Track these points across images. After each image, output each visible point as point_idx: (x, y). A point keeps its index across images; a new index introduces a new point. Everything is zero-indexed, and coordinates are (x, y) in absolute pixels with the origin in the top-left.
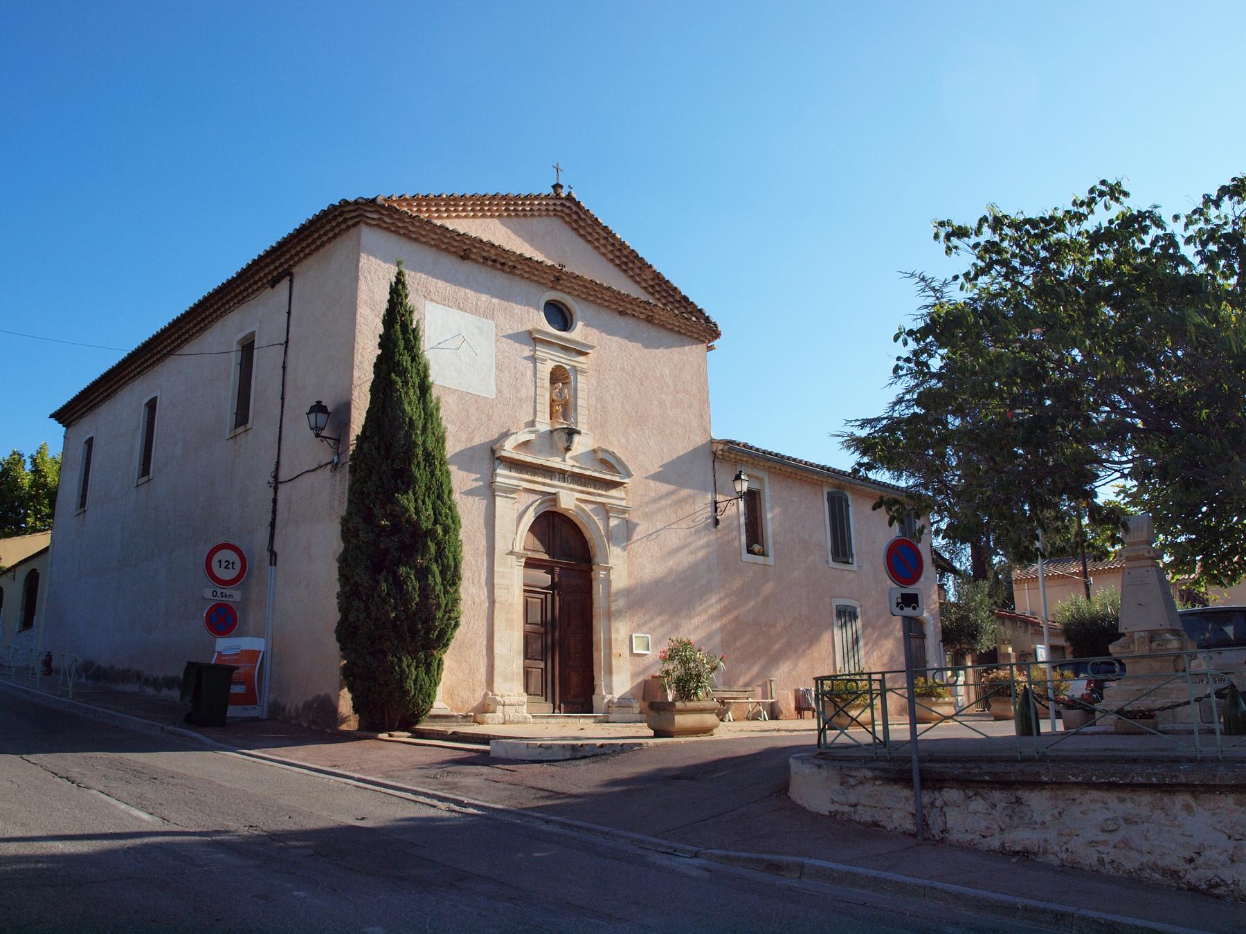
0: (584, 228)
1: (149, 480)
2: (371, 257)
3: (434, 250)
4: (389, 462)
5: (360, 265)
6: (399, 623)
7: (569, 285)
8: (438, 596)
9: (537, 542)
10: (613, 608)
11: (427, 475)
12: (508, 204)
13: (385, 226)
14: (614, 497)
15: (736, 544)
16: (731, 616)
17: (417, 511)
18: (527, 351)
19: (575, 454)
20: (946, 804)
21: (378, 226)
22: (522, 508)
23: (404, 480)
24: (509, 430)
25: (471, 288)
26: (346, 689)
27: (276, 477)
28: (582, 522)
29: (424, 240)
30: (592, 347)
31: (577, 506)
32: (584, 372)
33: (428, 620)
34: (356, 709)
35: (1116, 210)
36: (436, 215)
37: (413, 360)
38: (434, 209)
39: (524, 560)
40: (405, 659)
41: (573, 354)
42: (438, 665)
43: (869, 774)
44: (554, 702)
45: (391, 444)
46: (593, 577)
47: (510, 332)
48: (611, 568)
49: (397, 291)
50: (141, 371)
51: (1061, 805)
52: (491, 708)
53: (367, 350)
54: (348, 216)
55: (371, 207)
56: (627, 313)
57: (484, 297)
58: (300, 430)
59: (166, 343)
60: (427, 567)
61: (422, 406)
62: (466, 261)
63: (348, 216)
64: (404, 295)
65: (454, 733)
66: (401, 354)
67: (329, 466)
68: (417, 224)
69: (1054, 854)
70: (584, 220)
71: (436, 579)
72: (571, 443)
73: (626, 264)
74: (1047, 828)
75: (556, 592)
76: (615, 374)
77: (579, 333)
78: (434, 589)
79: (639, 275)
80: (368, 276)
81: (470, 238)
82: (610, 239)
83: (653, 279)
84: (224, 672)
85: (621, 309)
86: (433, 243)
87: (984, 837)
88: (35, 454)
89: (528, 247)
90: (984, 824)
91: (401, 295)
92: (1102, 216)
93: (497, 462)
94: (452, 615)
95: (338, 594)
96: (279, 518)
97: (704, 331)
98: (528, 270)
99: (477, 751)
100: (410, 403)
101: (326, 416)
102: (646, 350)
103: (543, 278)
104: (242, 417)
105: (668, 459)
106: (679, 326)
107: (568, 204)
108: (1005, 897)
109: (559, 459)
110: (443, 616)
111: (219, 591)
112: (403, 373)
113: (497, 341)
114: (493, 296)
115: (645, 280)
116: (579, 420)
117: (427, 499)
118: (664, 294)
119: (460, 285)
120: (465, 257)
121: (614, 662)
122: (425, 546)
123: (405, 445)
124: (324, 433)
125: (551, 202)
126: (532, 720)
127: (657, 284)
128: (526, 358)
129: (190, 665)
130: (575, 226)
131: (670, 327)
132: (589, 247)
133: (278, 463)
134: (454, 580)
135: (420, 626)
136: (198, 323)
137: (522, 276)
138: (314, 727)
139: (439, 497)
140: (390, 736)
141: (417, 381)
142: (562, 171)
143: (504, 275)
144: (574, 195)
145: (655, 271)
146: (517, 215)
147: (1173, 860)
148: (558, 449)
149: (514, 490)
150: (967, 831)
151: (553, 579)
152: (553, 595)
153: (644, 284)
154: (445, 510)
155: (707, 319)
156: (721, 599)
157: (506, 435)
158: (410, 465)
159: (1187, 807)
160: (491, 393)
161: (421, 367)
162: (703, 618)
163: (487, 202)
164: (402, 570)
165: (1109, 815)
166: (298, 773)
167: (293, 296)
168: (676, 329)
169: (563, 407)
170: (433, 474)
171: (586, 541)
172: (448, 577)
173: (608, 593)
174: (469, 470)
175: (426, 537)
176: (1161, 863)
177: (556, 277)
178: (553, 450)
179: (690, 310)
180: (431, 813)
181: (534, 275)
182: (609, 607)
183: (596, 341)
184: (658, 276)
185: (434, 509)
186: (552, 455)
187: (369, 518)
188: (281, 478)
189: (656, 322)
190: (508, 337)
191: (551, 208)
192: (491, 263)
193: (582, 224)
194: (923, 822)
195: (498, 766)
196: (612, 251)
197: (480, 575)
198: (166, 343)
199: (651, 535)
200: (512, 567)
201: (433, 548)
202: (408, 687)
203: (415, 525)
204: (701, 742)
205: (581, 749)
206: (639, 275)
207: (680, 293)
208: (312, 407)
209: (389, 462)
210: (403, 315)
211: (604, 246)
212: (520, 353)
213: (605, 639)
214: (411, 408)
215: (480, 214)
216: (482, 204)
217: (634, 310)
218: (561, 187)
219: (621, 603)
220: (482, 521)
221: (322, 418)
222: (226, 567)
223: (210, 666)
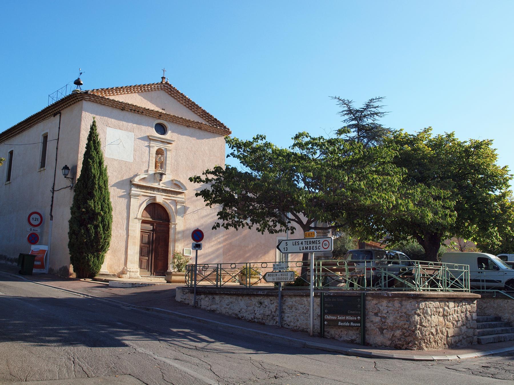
0: (173, 94)
1: (10, 183)
3: (111, 108)
4: (86, 189)
5: (82, 116)
7: (165, 117)
8: (101, 235)
9: (148, 214)
11: (99, 194)
12: (141, 88)
14: (179, 198)
16: (227, 242)
17: (95, 207)
18: (147, 143)
21: (89, 101)
23: (91, 196)
24: (138, 174)
25: (125, 121)
27: (53, 189)
29: (107, 104)
30: (174, 141)
31: (163, 201)
32: (170, 150)
33: (98, 242)
34: (74, 271)
37: (97, 153)
38: (111, 93)
39: (141, 221)
40: (89, 255)
41: (166, 143)
42: (102, 257)
43: (188, 291)
44: (151, 272)
47: (140, 137)
48: (177, 224)
49: (93, 128)
50: (7, 139)
51: (221, 299)
52: (125, 273)
53: (82, 149)
54: (78, 97)
57: (130, 124)
58: (60, 173)
59: (16, 130)
60: (98, 225)
63: (78, 97)
65: (105, 280)
66: (92, 152)
67: (70, 187)
68: (104, 99)
70: (173, 91)
71: (101, 229)
75: (154, 232)
76: (183, 150)
77: (169, 136)
78: (100, 232)
79: (197, 111)
81: (124, 103)
84: (32, 257)
85: (187, 125)
86: (110, 105)
89: (150, 103)
90: (208, 304)
91: (94, 130)
94: (107, 241)
96: (54, 203)
97: (224, 132)
99: (106, 284)
102: (198, 140)
103: (154, 115)
104: (43, 165)
106: (213, 130)
107: (166, 85)
111: (33, 229)
112: (92, 158)
113: (135, 140)
118: (207, 118)
119: (121, 120)
120: (123, 109)
122: (97, 218)
124: (67, 176)
125: (159, 86)
129: (21, 254)
130: (170, 93)
131: (209, 131)
132: (176, 101)
133: (54, 183)
136: (28, 125)
138: (62, 277)
139: (104, 201)
140: (85, 280)
141: (98, 161)
142: (166, 71)
143: (139, 115)
144: (169, 82)
148: (157, 180)
153: (199, 114)
154: (106, 205)
155: (225, 127)
156: (224, 236)
157: (136, 175)
159: (241, 300)
160: (131, 160)
161: (100, 156)
162: (216, 242)
163: (132, 88)
164: (89, 226)
165: (229, 301)
167: (61, 122)
168: (212, 131)
169: (160, 164)
172: (105, 228)
173: (175, 233)
175: (98, 215)
177: (160, 115)
178: (155, 181)
179: (218, 123)
180: (78, 297)
183: (176, 138)
185: (101, 206)
186: (154, 182)
187: (79, 208)
189: (203, 129)
190: (139, 139)
191: (160, 87)
192: (133, 111)
194: (196, 302)
196: (185, 102)
197: (123, 226)
198: (16, 130)
200: (136, 223)
203: (94, 211)
209: (86, 189)
210: (94, 137)
214: (95, 171)
215: (130, 92)
217: (193, 125)
218: (165, 78)
220: (125, 207)
221: (67, 171)
222: (35, 220)
223: (28, 255)
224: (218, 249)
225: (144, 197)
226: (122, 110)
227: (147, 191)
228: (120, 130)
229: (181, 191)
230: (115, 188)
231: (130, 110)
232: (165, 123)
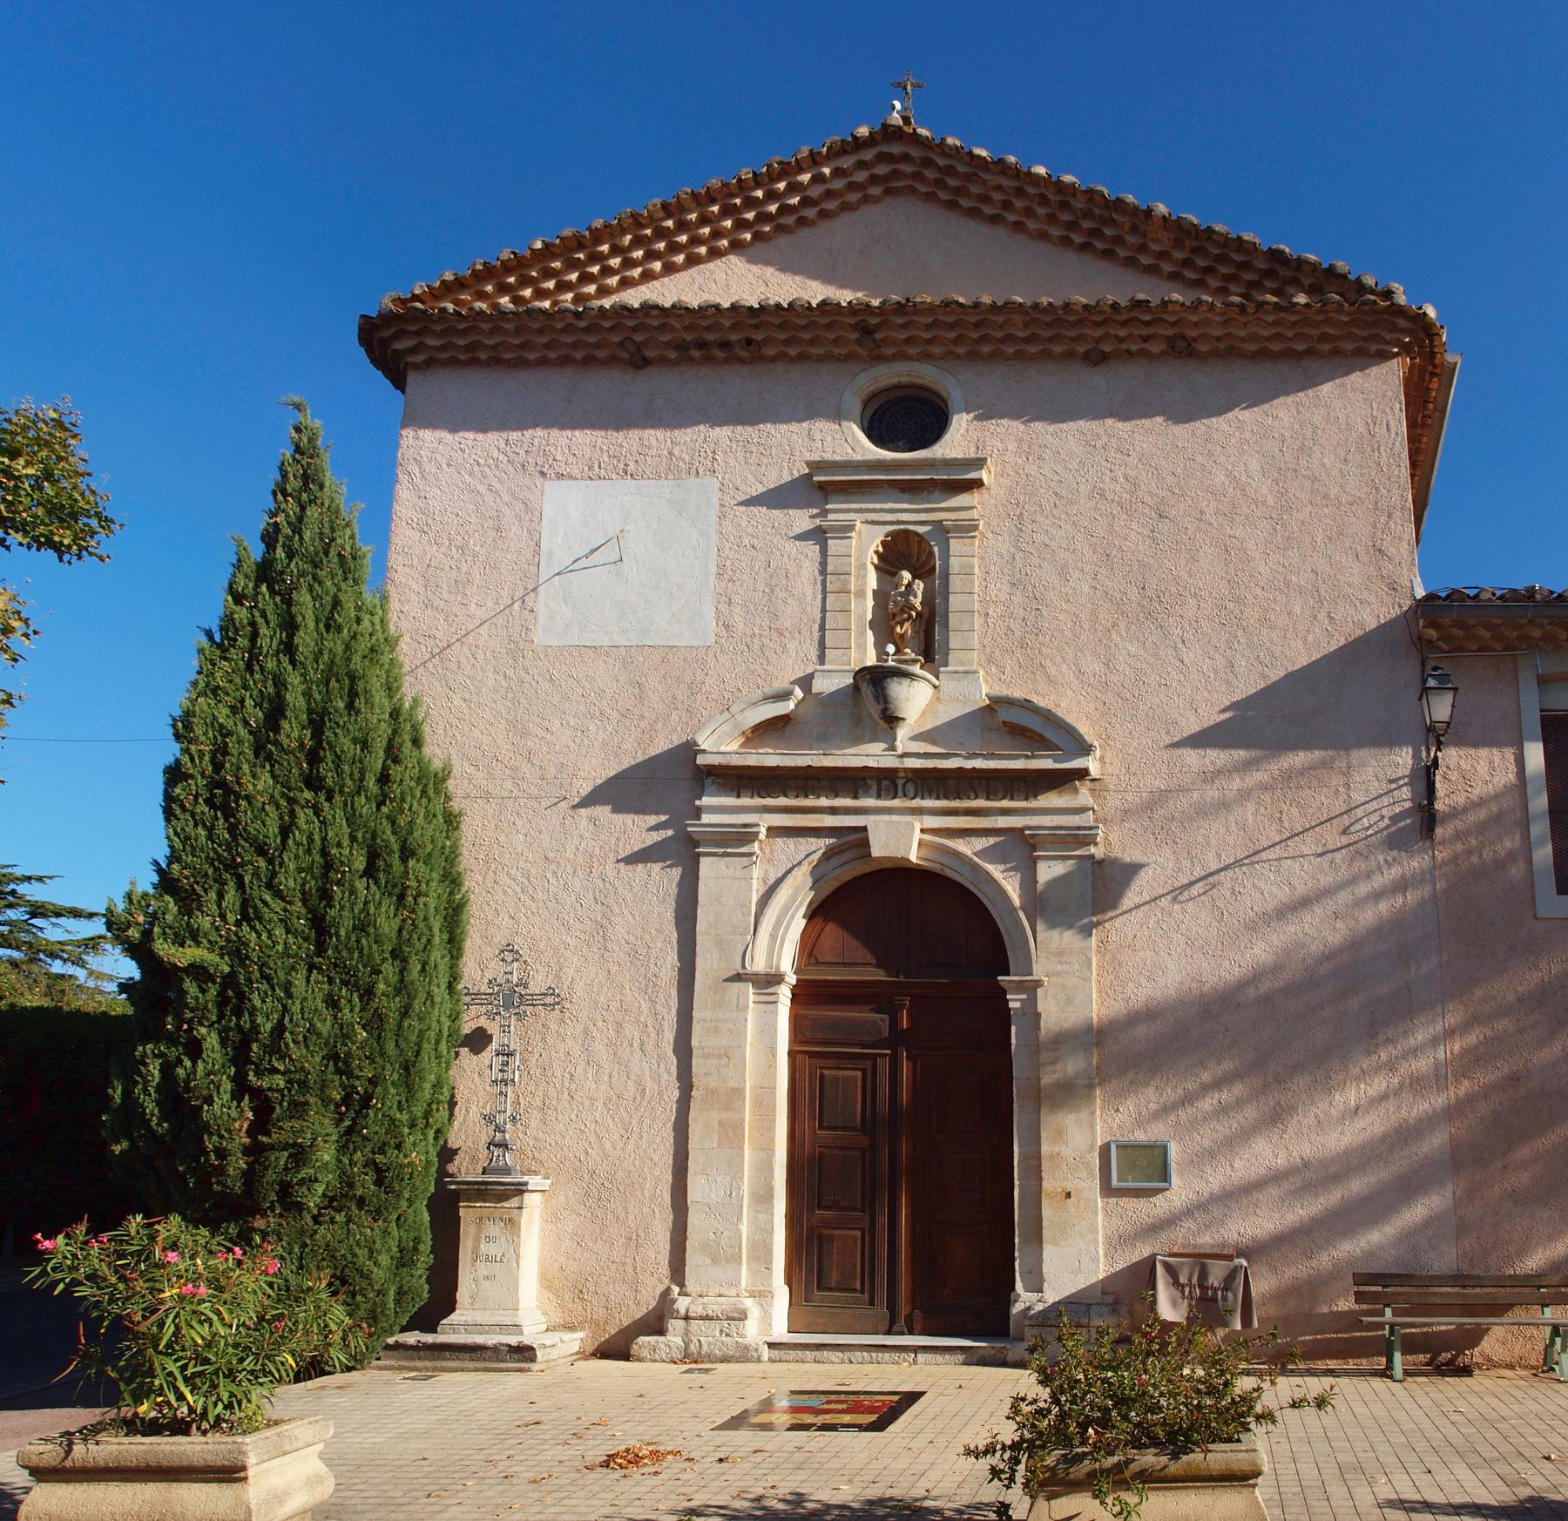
10: (1046, 1080)
15: (1516, 871)
16: (1485, 1077)
18: (802, 519)
30: (979, 463)
41: (937, 494)
62: (648, 370)
70: (949, 170)
73: (1096, 233)
82: (1031, 190)
88: (121, 906)
102: (1177, 429)
105: (1248, 686)
109: (878, 748)
113: (722, 516)
115: (1163, 255)
116: (951, 645)
120: (640, 362)
121: (1047, 1212)
131: (1252, 347)
132: (1001, 233)
146: (780, 229)
149: (745, 836)
151: (894, 1022)
168: (1276, 347)
173: (1034, 1045)
186: (859, 740)
189: (1203, 348)
206: (1143, 248)
211: (1029, 212)
224: (1402, 1136)
225: (791, 842)
227: (810, 802)
228: (630, 482)
229: (1047, 764)
230: (603, 812)
231: (673, 355)
232: (926, 374)
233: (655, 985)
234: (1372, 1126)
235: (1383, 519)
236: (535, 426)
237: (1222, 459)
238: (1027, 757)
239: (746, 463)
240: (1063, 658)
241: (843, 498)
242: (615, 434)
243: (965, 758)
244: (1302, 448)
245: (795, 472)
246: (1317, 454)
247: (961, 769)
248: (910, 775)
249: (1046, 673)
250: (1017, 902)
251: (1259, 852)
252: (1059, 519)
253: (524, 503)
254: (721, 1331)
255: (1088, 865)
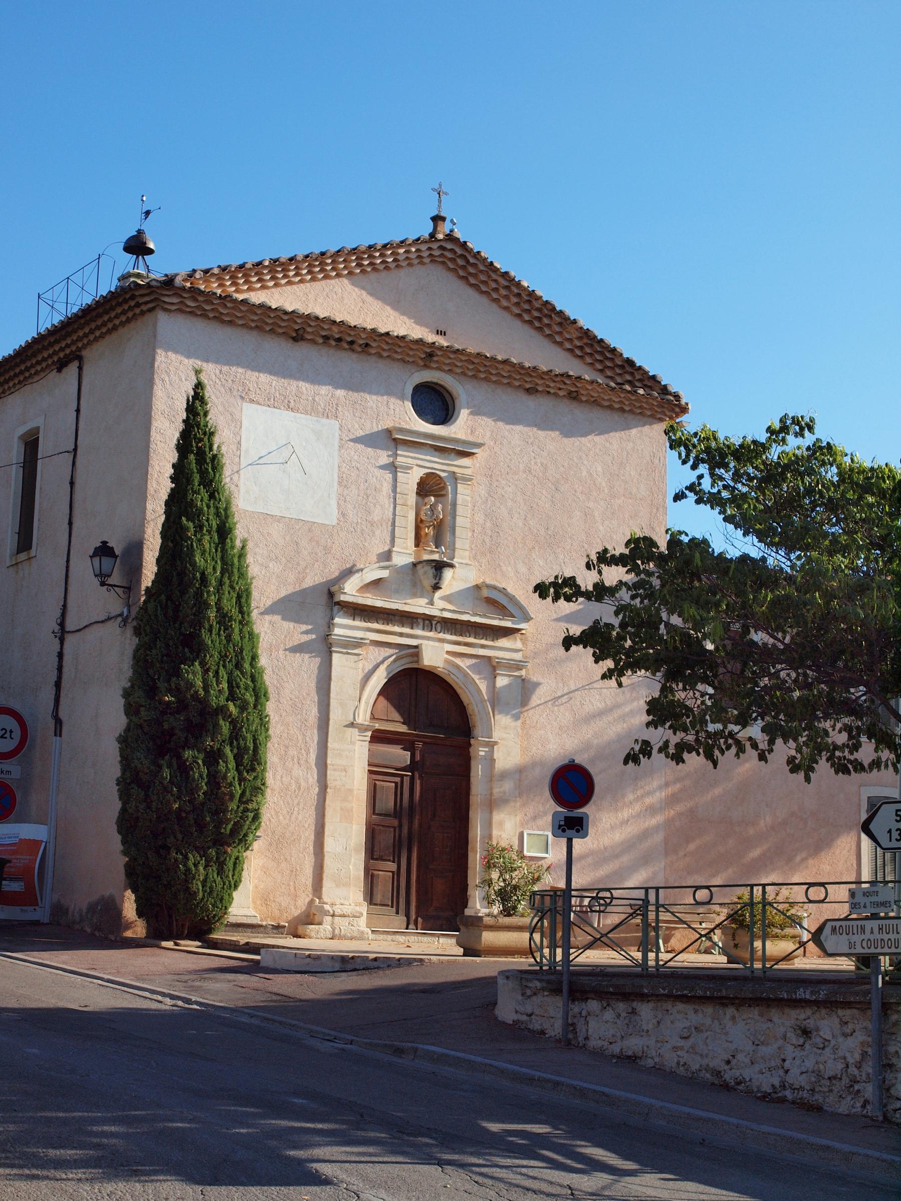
0: (475, 276)
2: (170, 353)
3: (255, 333)
5: (156, 364)
6: (184, 815)
7: (447, 361)
12: (359, 258)
13: (188, 310)
16: (680, 808)
17: (206, 688)
18: (384, 457)
19: (448, 593)
20: (589, 1014)
21: (180, 311)
22: (369, 667)
24: (354, 565)
25: (306, 379)
26: (129, 891)
27: (62, 624)
28: (456, 683)
29: (240, 322)
30: (479, 445)
31: (446, 661)
32: (467, 479)
33: (219, 811)
34: (140, 913)
35: (809, 439)
36: (259, 285)
37: (212, 496)
39: (369, 734)
40: (190, 856)
42: (235, 864)
44: (407, 915)
45: (180, 604)
46: (472, 754)
47: (360, 433)
48: (496, 743)
52: (317, 919)
54: (141, 300)
55: (167, 290)
56: (537, 391)
57: (324, 390)
60: (219, 750)
61: (219, 554)
62: (300, 343)
63: (141, 300)
64: (202, 414)
65: (247, 943)
66: (194, 492)
68: (229, 305)
69: (652, 1058)
70: (474, 265)
71: (228, 766)
72: (440, 579)
73: (539, 319)
74: (650, 1036)
75: (417, 775)
76: (516, 477)
78: (225, 777)
80: (167, 379)
81: (301, 316)
83: (580, 338)
85: (528, 386)
87: (611, 1043)
91: (199, 414)
92: (795, 444)
93: (336, 608)
94: (250, 806)
95: (118, 780)
96: (65, 676)
98: (386, 347)
99: (252, 960)
100: (203, 553)
101: (112, 560)
102: (566, 441)
103: (408, 355)
104: (24, 541)
107: (449, 246)
108: (524, 1070)
109: (423, 601)
110: (238, 807)
112: (195, 515)
113: (341, 447)
114: (337, 386)
116: (457, 546)
117: (221, 668)
118: (598, 357)
120: (298, 337)
122: (216, 725)
123: (195, 605)
125: (424, 247)
126: (371, 936)
127: (586, 344)
128: (382, 467)
130: (461, 273)
131: (607, 404)
132: (484, 300)
133: (65, 606)
134: (252, 765)
135: (208, 819)
137: (380, 356)
138: (97, 933)
139: (238, 666)
140: (176, 944)
141: (214, 524)
142: (446, 194)
144: (458, 234)
145: (581, 328)
147: (717, 1063)
148: (423, 587)
149: (358, 644)
150: (600, 1038)
151: (413, 756)
152: (412, 778)
153: (568, 346)
155: (664, 390)
156: (667, 785)
157: (349, 572)
158: (200, 630)
159: (733, 1018)
160: (330, 517)
162: (637, 807)
164: (188, 754)
165: (687, 1024)
166: (51, 973)
170: (229, 638)
171: (465, 707)
173: (491, 777)
174: (298, 621)
175: (217, 715)
176: (711, 1065)
178: (415, 589)
180: (154, 1006)
181: (396, 352)
182: (491, 794)
183: (488, 434)
184: (587, 334)
185: (229, 682)
186: (414, 595)
187: (152, 691)
188: (69, 626)
189: (584, 399)
190: (357, 440)
193: (471, 270)
195: (259, 975)
196: (517, 304)
197: (308, 753)
199: (559, 697)
200: (352, 743)
201: (225, 727)
202: (194, 889)
203: (204, 702)
204: (489, 962)
205: (351, 961)
207: (621, 355)
208: (96, 549)
210: (201, 440)
211: (507, 297)
212: (373, 461)
213: (482, 837)
216: (322, 264)
218: (443, 219)
219: (508, 786)
220: (313, 685)
221: (107, 561)
224: (645, 835)
226: (295, 339)
227: (389, 628)
228: (290, 413)
233: (306, 726)
234: (631, 830)
235: (655, 511)
236: (238, 365)
237: (585, 462)
238: (500, 619)
239: (354, 415)
240: (509, 562)
241: (406, 448)
242: (283, 380)
243: (471, 615)
244: (622, 463)
245: (380, 427)
246: (628, 468)
247: (469, 621)
248: (440, 620)
249: (501, 570)
250: (486, 698)
251: (592, 683)
252: (509, 481)
253: (231, 414)
254: (349, 923)
255: (519, 681)
